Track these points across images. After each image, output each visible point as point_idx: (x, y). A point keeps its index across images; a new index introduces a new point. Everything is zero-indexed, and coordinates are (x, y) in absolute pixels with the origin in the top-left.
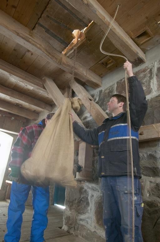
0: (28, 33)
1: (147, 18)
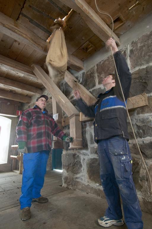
0: (13, 24)
1: (119, 5)
